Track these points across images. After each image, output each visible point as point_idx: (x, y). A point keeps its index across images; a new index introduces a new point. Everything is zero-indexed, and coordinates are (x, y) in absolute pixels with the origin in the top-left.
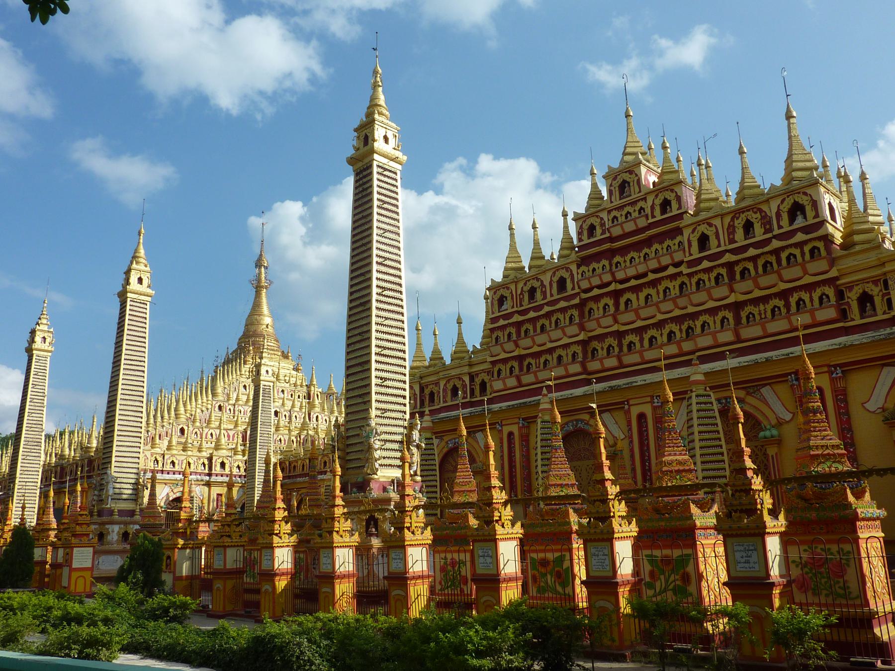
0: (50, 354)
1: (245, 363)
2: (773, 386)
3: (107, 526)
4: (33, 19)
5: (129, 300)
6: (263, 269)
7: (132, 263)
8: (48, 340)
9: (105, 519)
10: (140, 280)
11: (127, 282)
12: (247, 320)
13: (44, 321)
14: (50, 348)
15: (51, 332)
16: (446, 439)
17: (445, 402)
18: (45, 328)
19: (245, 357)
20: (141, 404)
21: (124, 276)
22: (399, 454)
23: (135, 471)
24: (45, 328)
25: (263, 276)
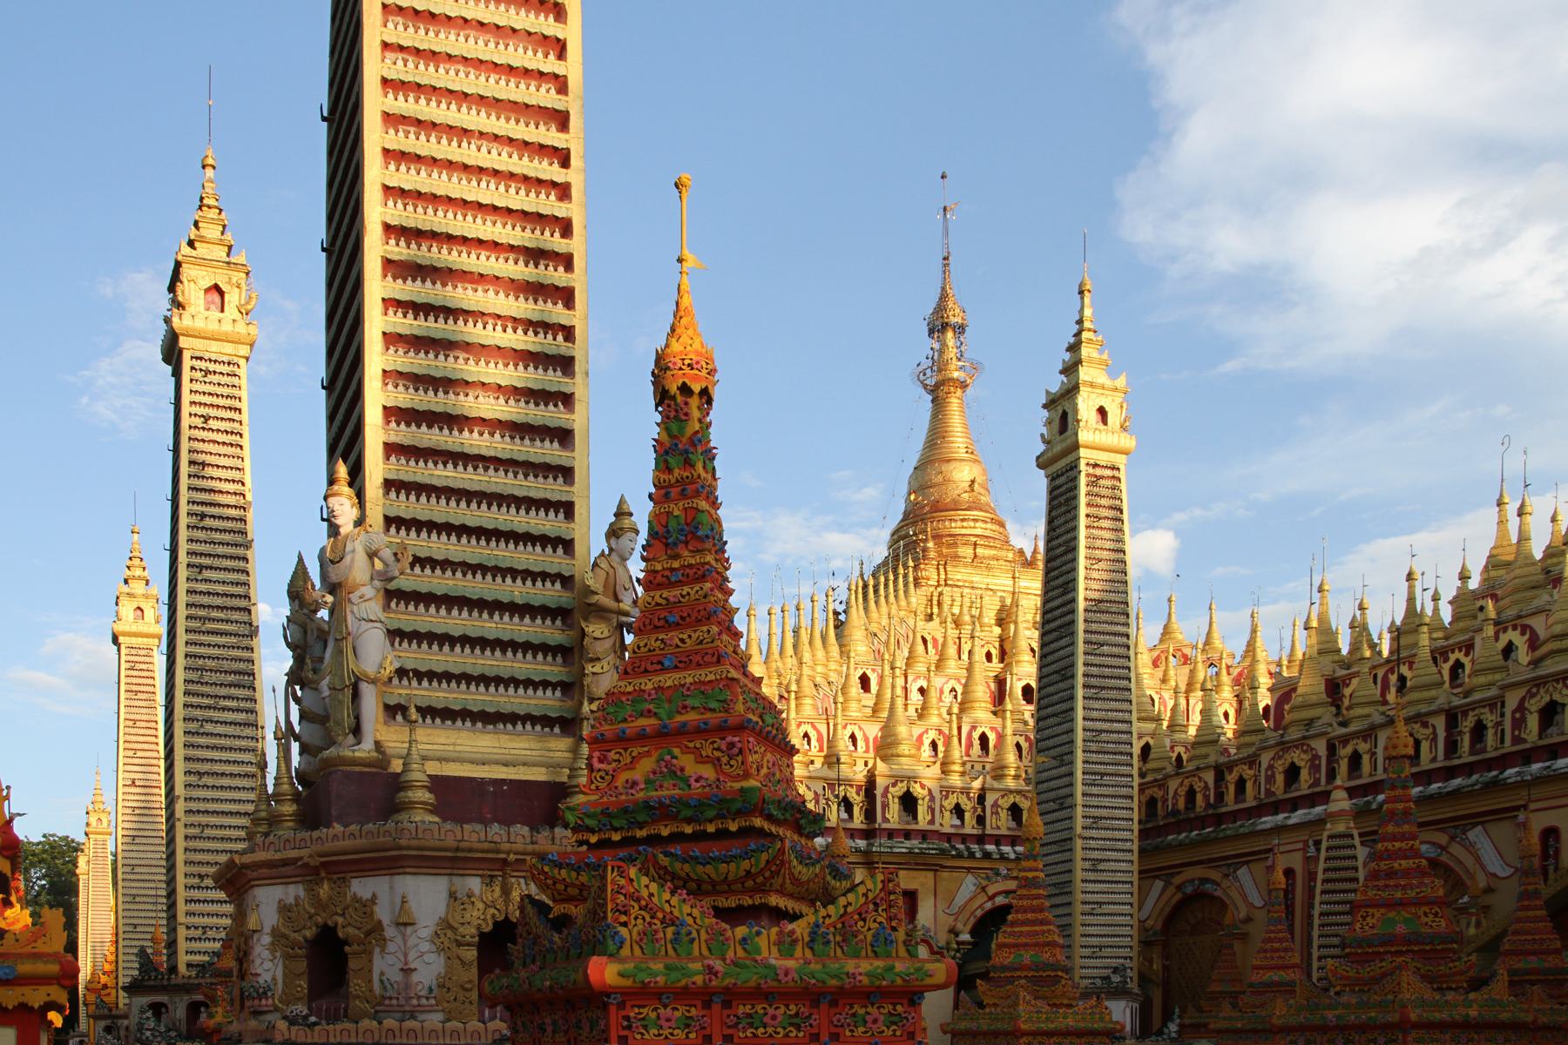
1: (917, 584)
2: (1489, 827)
3: (361, 887)
4: (385, 276)
6: (950, 334)
9: (338, 836)
16: (1177, 880)
19: (916, 567)
25: (952, 352)
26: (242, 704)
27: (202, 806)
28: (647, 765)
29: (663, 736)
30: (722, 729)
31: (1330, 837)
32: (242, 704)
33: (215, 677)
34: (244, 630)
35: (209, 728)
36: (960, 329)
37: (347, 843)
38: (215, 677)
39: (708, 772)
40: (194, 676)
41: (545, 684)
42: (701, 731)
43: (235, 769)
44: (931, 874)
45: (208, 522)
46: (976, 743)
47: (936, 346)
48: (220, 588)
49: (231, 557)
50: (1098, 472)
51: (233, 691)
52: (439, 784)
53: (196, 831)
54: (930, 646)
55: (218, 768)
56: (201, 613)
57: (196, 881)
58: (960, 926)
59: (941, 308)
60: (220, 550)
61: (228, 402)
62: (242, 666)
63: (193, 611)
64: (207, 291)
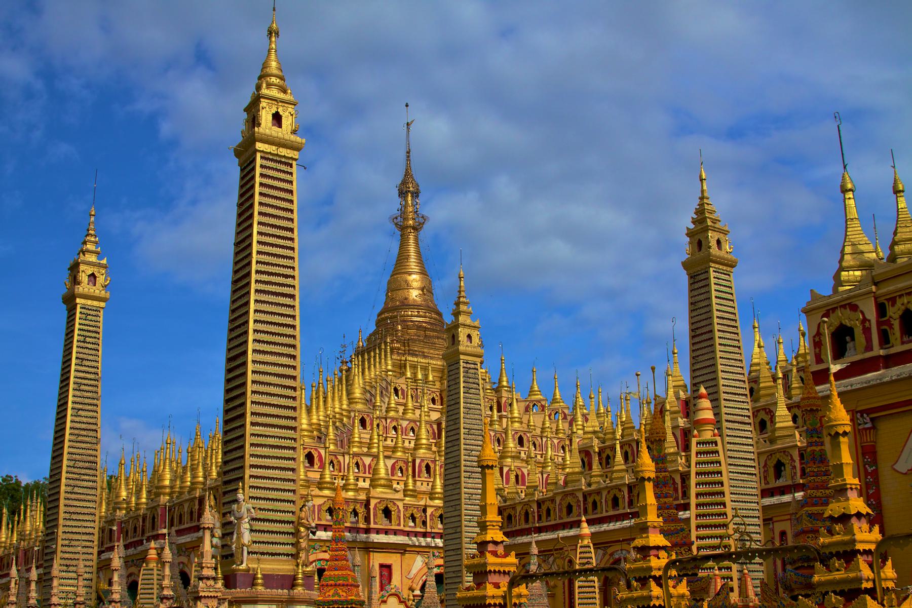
0: (103, 304)
5: (79, 306)
7: (259, 88)
8: (101, 279)
10: (277, 119)
11: (254, 121)
12: (389, 282)
13: (90, 247)
14: (103, 294)
15: (105, 267)
17: (561, 518)
18: (93, 258)
20: (290, 362)
21: (245, 115)
22: (290, 539)
23: (289, 528)
24: (93, 258)
26: (91, 478)
27: (70, 530)
28: (331, 593)
29: (336, 585)
30: (347, 585)
31: (581, 547)
32: (91, 478)
33: (81, 464)
34: (94, 441)
35: (76, 490)
36: (416, 195)
37: (247, 595)
38: (81, 464)
39: (344, 594)
40: (72, 463)
41: (288, 544)
42: (343, 585)
43: (86, 511)
44: (399, 555)
45: (83, 387)
46: (424, 469)
47: (404, 203)
48: (85, 420)
49: (91, 405)
50: (468, 366)
51: (87, 471)
52: (265, 577)
53: (67, 542)
54: (400, 393)
55: (78, 510)
56: (76, 432)
57: (65, 568)
58: (414, 586)
59: (404, 183)
60: (87, 401)
61: (94, 329)
62: (91, 458)
63: (73, 431)
64: (89, 276)
